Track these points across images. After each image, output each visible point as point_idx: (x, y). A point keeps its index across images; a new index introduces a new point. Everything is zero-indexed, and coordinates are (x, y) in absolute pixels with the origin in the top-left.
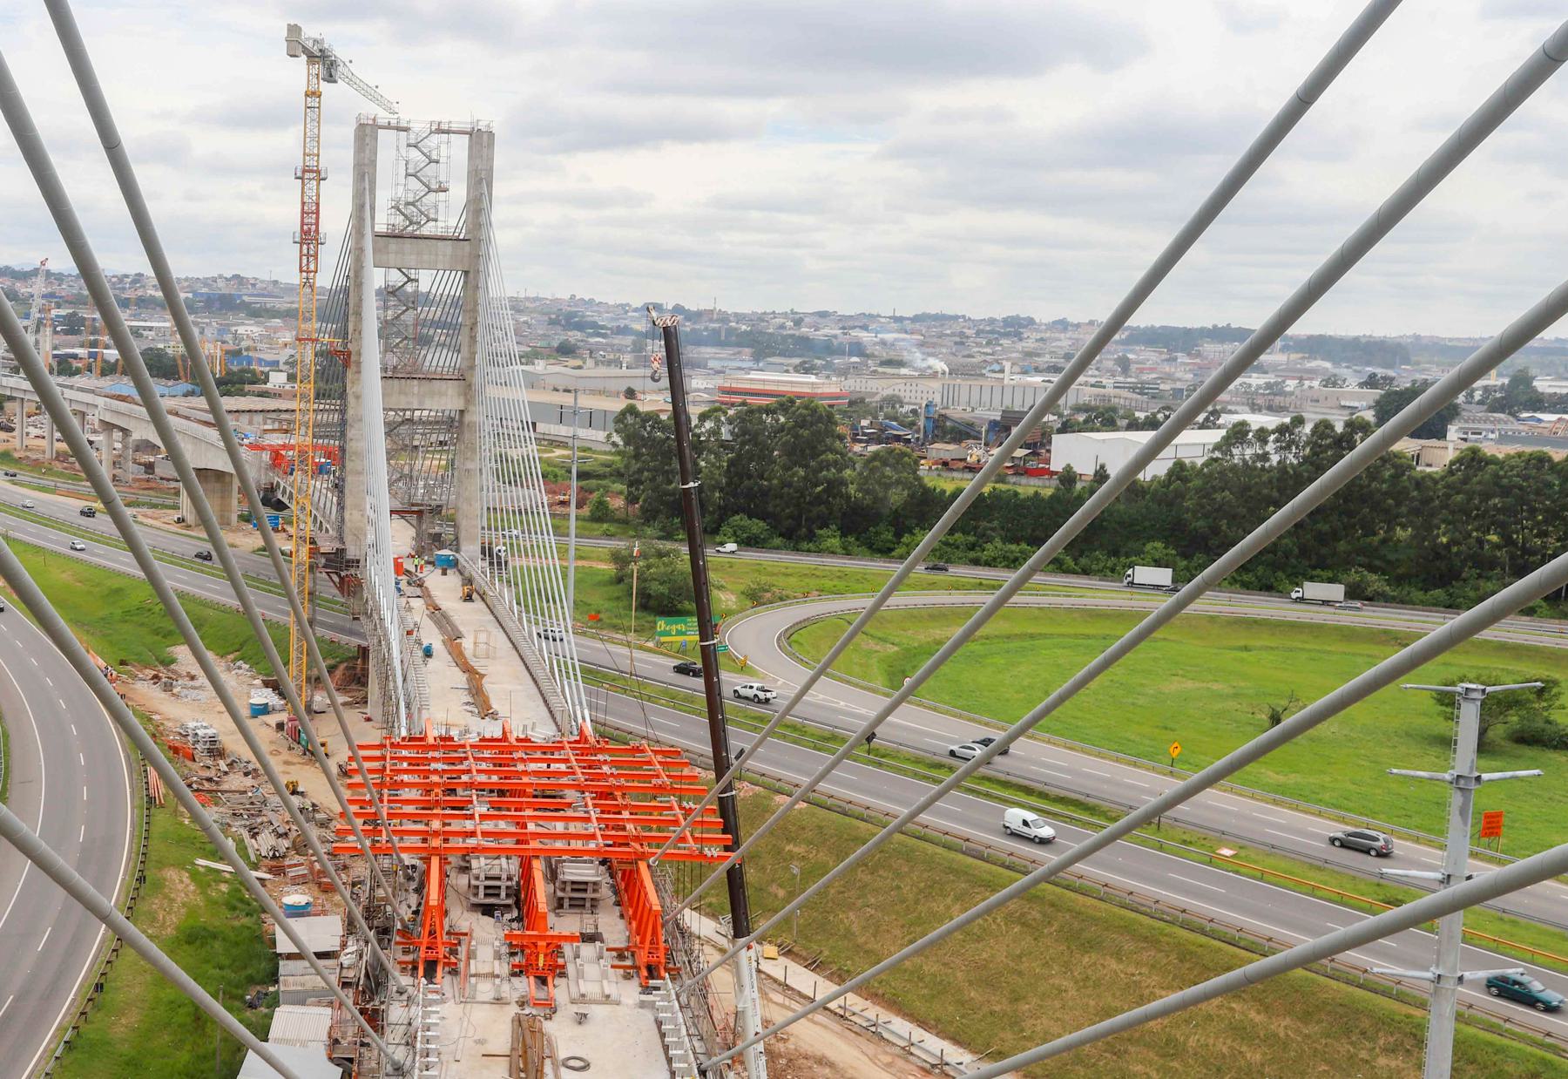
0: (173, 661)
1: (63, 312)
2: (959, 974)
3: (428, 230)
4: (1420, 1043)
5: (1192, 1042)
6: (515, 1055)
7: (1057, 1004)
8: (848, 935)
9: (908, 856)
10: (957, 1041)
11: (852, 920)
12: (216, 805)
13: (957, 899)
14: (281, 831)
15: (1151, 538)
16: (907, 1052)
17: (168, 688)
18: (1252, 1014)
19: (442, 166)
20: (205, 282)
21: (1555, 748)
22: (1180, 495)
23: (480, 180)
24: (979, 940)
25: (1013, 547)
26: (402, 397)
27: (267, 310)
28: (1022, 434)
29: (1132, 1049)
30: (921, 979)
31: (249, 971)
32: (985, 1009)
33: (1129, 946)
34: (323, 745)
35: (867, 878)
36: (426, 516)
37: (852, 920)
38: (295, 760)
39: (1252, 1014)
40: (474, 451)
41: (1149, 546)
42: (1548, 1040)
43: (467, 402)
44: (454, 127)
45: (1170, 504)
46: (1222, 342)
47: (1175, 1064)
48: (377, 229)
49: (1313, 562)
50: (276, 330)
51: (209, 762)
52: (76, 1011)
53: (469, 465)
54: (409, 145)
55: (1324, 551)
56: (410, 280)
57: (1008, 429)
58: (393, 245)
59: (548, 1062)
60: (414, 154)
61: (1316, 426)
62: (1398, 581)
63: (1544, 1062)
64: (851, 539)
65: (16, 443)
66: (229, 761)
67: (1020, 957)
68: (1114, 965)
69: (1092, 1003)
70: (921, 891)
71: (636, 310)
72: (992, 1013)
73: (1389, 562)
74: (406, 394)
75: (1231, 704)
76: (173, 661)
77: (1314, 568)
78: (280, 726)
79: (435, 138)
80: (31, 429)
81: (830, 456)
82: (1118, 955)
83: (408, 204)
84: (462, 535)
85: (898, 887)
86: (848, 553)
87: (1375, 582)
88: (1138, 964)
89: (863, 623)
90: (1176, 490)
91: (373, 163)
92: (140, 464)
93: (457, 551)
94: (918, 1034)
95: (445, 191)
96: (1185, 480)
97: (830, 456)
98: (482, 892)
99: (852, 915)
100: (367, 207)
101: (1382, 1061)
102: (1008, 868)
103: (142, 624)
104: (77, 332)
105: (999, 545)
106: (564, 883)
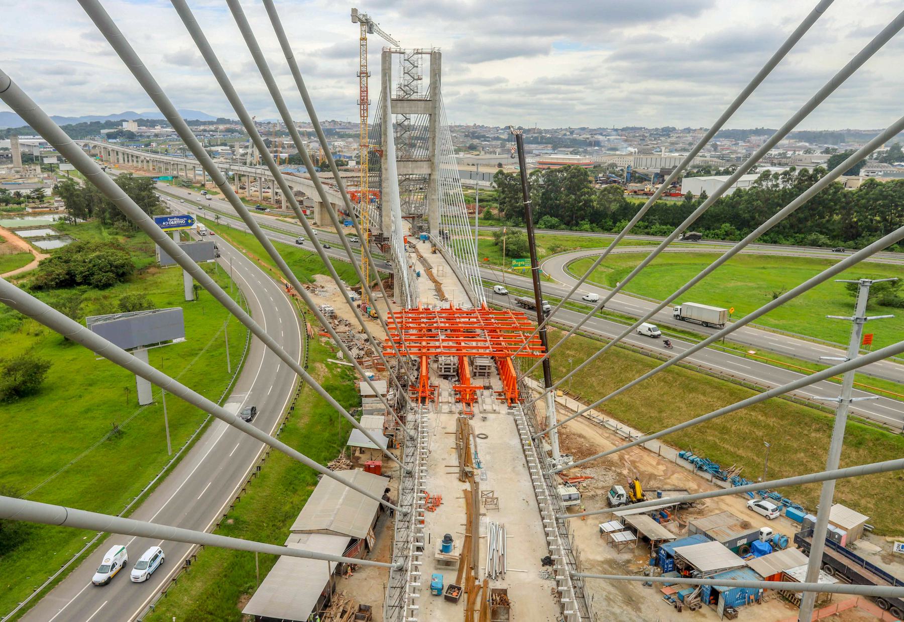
0: (315, 281)
2: (637, 402)
3: (414, 97)
5: (734, 428)
6: (458, 433)
7: (678, 413)
8: (592, 386)
9: (617, 355)
14: (361, 347)
15: (725, 222)
16: (615, 432)
18: (760, 417)
19: (419, 69)
23: (436, 73)
24: (646, 388)
25: (664, 227)
27: (346, 135)
30: (622, 404)
31: (350, 402)
32: (648, 416)
33: (709, 390)
35: (600, 364)
36: (416, 219)
37: (593, 381)
40: (435, 191)
41: (723, 226)
43: (432, 170)
46: (759, 135)
47: (726, 437)
48: (392, 97)
49: (796, 230)
50: (350, 143)
52: (284, 417)
53: (433, 197)
55: (800, 226)
56: (407, 119)
58: (399, 104)
61: (801, 171)
62: (833, 238)
64: (594, 225)
67: (664, 394)
68: (702, 398)
69: (692, 413)
70: (622, 369)
71: (502, 129)
72: (651, 417)
75: (757, 292)
76: (315, 281)
77: (796, 233)
79: (416, 56)
80: (252, 188)
81: (586, 190)
82: (704, 394)
83: (405, 86)
85: (613, 368)
88: (712, 397)
90: (736, 201)
91: (390, 69)
93: (429, 233)
94: (620, 425)
95: (421, 79)
97: (586, 190)
99: (593, 379)
101: (813, 435)
102: (659, 359)
103: (301, 266)
105: (658, 226)
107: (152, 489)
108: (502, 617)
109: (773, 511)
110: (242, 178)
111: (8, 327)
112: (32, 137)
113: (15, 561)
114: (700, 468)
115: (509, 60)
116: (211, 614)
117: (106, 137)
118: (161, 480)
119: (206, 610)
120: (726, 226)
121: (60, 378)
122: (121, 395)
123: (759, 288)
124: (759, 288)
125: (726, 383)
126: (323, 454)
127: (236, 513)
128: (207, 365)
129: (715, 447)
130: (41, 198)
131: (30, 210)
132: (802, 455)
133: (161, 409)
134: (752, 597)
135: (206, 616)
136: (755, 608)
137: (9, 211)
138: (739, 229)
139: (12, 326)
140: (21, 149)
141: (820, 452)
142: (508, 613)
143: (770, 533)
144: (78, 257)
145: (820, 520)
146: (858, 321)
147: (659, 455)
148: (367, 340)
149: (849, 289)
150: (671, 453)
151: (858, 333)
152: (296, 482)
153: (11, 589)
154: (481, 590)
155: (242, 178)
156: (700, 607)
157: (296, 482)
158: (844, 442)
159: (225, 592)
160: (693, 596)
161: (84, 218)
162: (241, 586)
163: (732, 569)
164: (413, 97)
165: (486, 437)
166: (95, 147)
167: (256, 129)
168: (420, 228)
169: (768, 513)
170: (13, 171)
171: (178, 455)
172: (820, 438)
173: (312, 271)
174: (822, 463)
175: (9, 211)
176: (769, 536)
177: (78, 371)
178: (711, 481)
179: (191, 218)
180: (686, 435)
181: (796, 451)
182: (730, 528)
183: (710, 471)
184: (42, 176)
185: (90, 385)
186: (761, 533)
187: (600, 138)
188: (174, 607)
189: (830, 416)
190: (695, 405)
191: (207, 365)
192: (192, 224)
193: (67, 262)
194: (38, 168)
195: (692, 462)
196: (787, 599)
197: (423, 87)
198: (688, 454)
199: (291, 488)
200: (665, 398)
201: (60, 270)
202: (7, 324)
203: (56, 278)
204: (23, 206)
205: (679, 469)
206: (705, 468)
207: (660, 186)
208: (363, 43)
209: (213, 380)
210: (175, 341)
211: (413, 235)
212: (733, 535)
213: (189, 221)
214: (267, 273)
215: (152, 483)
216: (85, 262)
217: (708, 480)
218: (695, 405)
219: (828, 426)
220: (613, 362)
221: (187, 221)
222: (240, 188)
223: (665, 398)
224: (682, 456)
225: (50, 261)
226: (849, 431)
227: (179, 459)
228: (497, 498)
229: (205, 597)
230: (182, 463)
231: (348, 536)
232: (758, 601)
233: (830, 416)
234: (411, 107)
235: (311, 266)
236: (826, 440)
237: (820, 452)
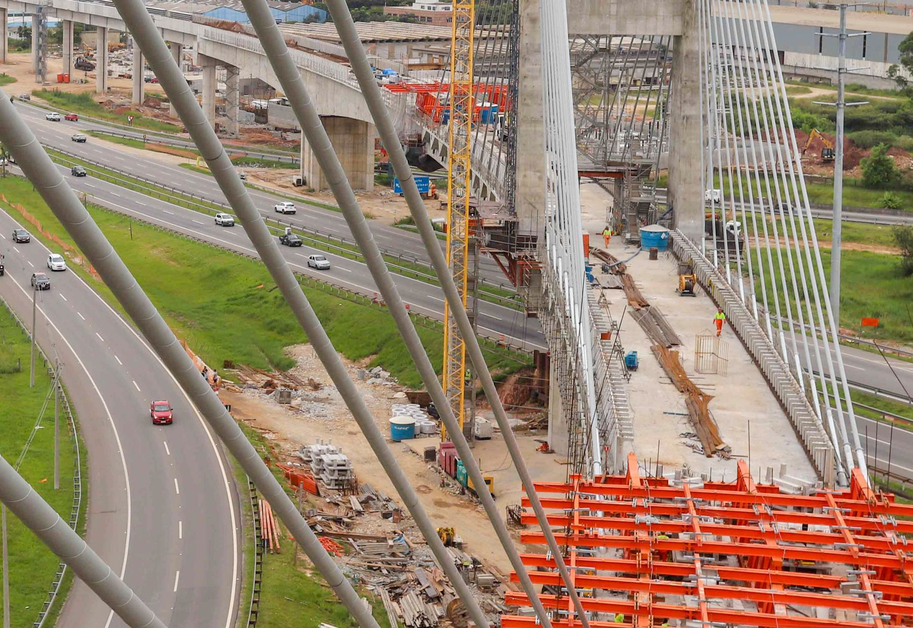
0: (291, 364)
12: (347, 553)
14: (431, 593)
17: (285, 398)
26: (595, 20)
34: (488, 482)
36: (628, 180)
38: (450, 500)
40: (694, 91)
43: (686, 24)
51: (338, 498)
53: (689, 110)
65: (97, 84)
66: (363, 497)
74: (600, 15)
76: (291, 364)
78: (430, 455)
84: (679, 206)
92: (249, 110)
93: (672, 226)
103: (252, 316)
110: (86, 37)
155: (86, 37)
222: (79, 66)
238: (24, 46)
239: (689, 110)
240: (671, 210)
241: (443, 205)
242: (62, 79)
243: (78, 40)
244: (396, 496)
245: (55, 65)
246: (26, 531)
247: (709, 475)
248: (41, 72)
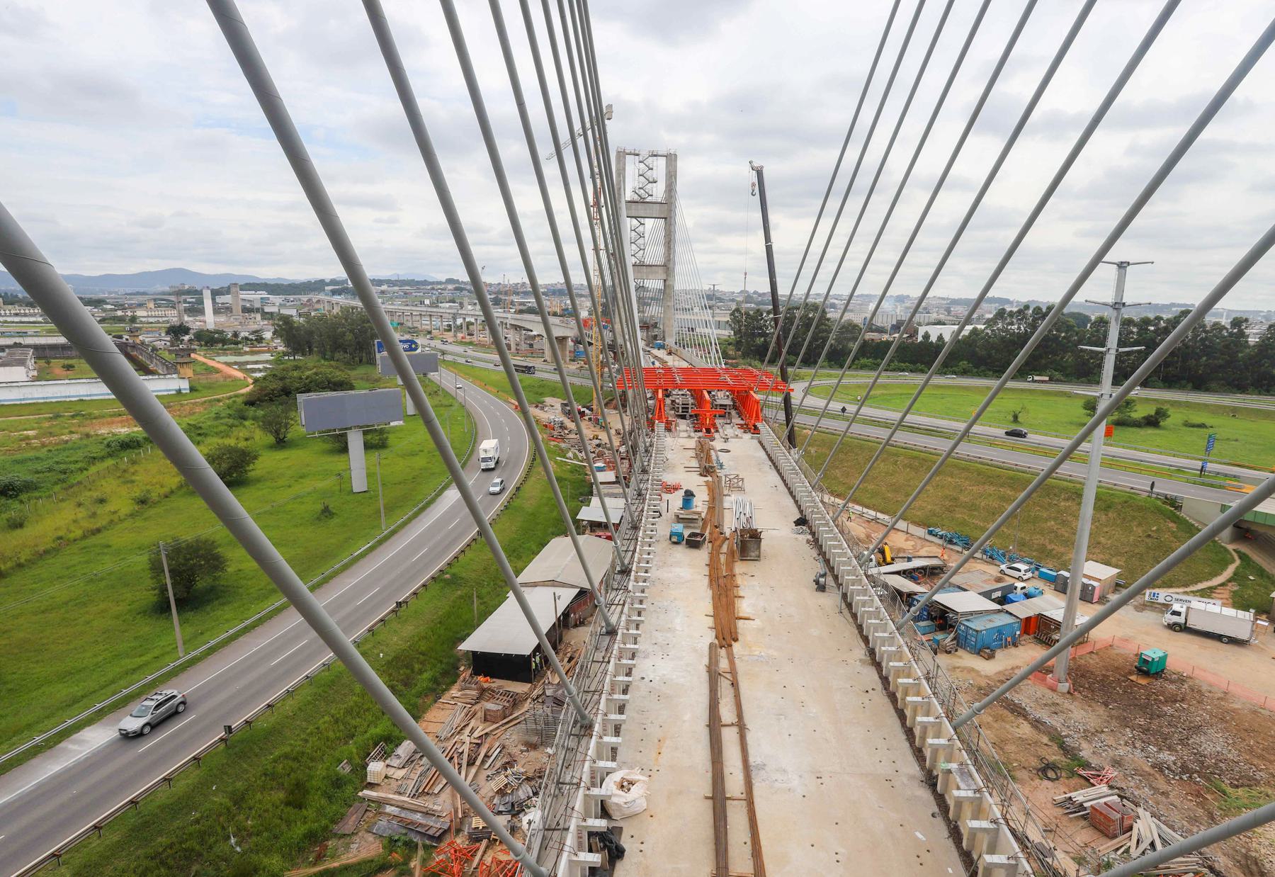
1: (492, 297)
3: (649, 199)
4: (1080, 495)
5: (983, 504)
6: (698, 449)
8: (836, 478)
9: (861, 447)
10: (882, 512)
11: (838, 473)
13: (883, 461)
15: (962, 360)
16: (861, 515)
17: (542, 409)
18: (1008, 492)
19: (654, 171)
20: (552, 285)
21: (1132, 426)
22: (974, 341)
23: (671, 176)
24: (892, 475)
28: (905, 329)
29: (957, 509)
31: (581, 491)
35: (844, 457)
37: (838, 473)
39: (1008, 492)
42: (1132, 491)
43: (667, 276)
44: (660, 153)
45: (970, 346)
52: (509, 497)
53: (669, 304)
54: (640, 162)
57: (900, 328)
59: (712, 451)
60: (642, 165)
62: (1067, 376)
63: (1130, 497)
65: (475, 339)
73: (1062, 367)
78: (590, 419)
81: (824, 327)
83: (640, 188)
86: (831, 367)
87: (1057, 375)
89: (837, 387)
91: (624, 169)
96: (977, 335)
97: (824, 327)
98: (680, 410)
100: (622, 189)
101: (1062, 504)
104: (499, 304)
106: (716, 405)
107: (362, 556)
108: (753, 554)
109: (1026, 571)
110: (471, 327)
111: (216, 433)
112: (253, 292)
113: (208, 614)
114: (950, 542)
115: (710, 775)
116: (423, 655)
117: (331, 294)
118: (372, 549)
119: (417, 650)
120: (964, 364)
121: (268, 473)
122: (334, 485)
123: (999, 412)
124: (999, 412)
125: (972, 464)
126: (551, 530)
127: (454, 570)
128: (428, 463)
129: (964, 523)
130: (260, 340)
131: (248, 349)
132: (1053, 523)
133: (377, 496)
134: (1009, 639)
135: (417, 656)
136: (1013, 650)
137: (225, 350)
138: (975, 367)
139: (221, 432)
140: (242, 303)
141: (1070, 518)
142: (759, 547)
143: (1024, 588)
144: (295, 374)
145: (1074, 577)
146: (1117, 306)
147: (908, 533)
148: (599, 445)
149: (1085, 408)
150: (921, 532)
151: (1116, 319)
152: (521, 550)
153: (202, 633)
154: (727, 542)
155: (471, 327)
156: (956, 650)
157: (521, 550)
158: (1095, 508)
159: (439, 637)
160: (949, 639)
161: (303, 355)
162: (457, 633)
163: (988, 612)
164: (647, 200)
165: (729, 451)
166: (318, 301)
167: (485, 289)
168: (655, 337)
169: (1021, 574)
170: (232, 319)
171: (392, 527)
172: (1069, 506)
173: (542, 394)
174: (1072, 528)
175: (225, 350)
176: (1023, 591)
177: (289, 468)
178: (962, 553)
179: (415, 343)
180: (935, 515)
181: (1046, 520)
182: (985, 581)
183: (960, 543)
184: (262, 323)
185: (301, 477)
186: (1016, 588)
187: (836, 301)
188: (382, 645)
189: (1078, 486)
190: (942, 487)
191: (428, 463)
192: (416, 349)
193: (282, 379)
194: (258, 316)
195: (941, 537)
196: (1044, 642)
197: (658, 192)
198: (937, 530)
199: (515, 554)
200: (911, 483)
201: (275, 385)
202: (215, 430)
203: (270, 394)
204: (240, 346)
205: (928, 544)
206: (955, 541)
207: (897, 335)
208: (581, 840)
209: (433, 474)
210: (392, 424)
211: (647, 345)
212: (988, 588)
213: (413, 346)
214: (494, 395)
215: (363, 549)
216: (301, 378)
217: (958, 552)
218: (942, 487)
219: (1077, 495)
220: (857, 454)
221: (410, 346)
223: (911, 483)
224: (930, 533)
225: (264, 378)
226: (1098, 498)
227: (393, 533)
228: (742, 479)
229: (416, 639)
230: (396, 536)
231: (576, 587)
232: (1015, 645)
233: (1078, 486)
234: (646, 210)
235: (540, 390)
236: (1075, 508)
237: (1070, 518)
238: (450, 330)
239: (669, 304)
240: (664, 337)
241: (636, 639)
242: (463, 338)
243: (468, 328)
244: (608, 442)
245: (460, 335)
246: (914, 407)
247: (621, 428)
248: (455, 336)
